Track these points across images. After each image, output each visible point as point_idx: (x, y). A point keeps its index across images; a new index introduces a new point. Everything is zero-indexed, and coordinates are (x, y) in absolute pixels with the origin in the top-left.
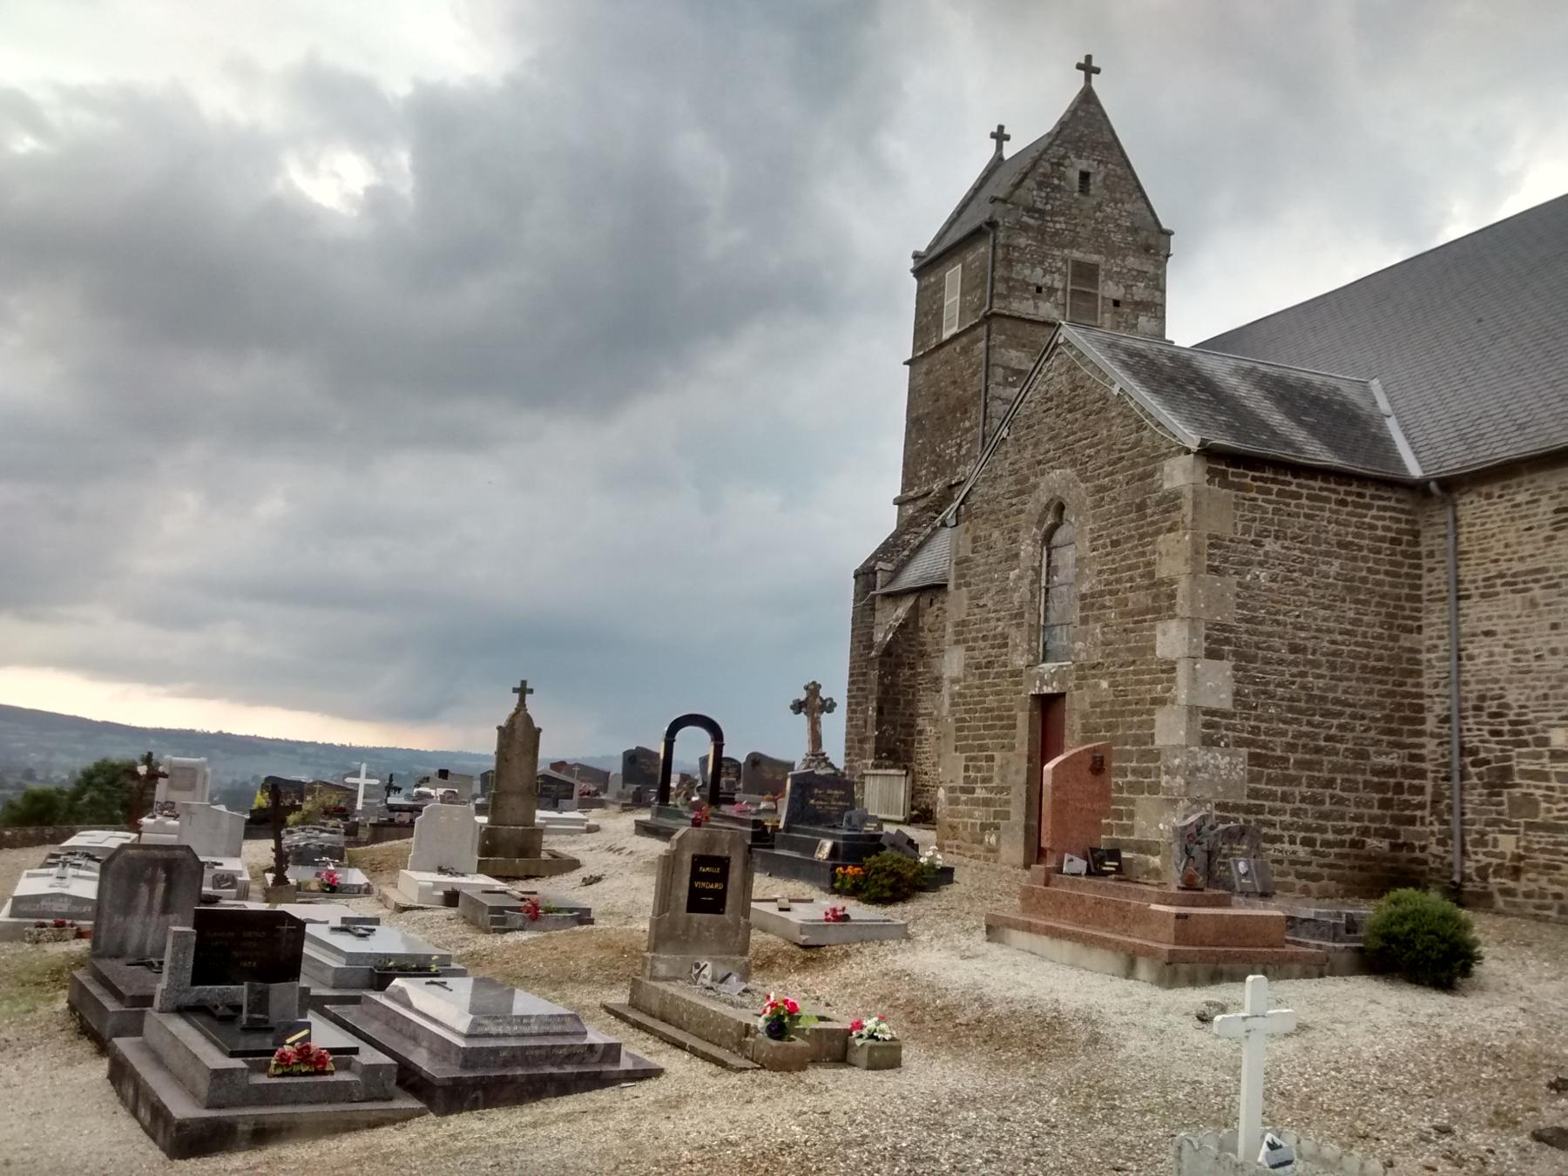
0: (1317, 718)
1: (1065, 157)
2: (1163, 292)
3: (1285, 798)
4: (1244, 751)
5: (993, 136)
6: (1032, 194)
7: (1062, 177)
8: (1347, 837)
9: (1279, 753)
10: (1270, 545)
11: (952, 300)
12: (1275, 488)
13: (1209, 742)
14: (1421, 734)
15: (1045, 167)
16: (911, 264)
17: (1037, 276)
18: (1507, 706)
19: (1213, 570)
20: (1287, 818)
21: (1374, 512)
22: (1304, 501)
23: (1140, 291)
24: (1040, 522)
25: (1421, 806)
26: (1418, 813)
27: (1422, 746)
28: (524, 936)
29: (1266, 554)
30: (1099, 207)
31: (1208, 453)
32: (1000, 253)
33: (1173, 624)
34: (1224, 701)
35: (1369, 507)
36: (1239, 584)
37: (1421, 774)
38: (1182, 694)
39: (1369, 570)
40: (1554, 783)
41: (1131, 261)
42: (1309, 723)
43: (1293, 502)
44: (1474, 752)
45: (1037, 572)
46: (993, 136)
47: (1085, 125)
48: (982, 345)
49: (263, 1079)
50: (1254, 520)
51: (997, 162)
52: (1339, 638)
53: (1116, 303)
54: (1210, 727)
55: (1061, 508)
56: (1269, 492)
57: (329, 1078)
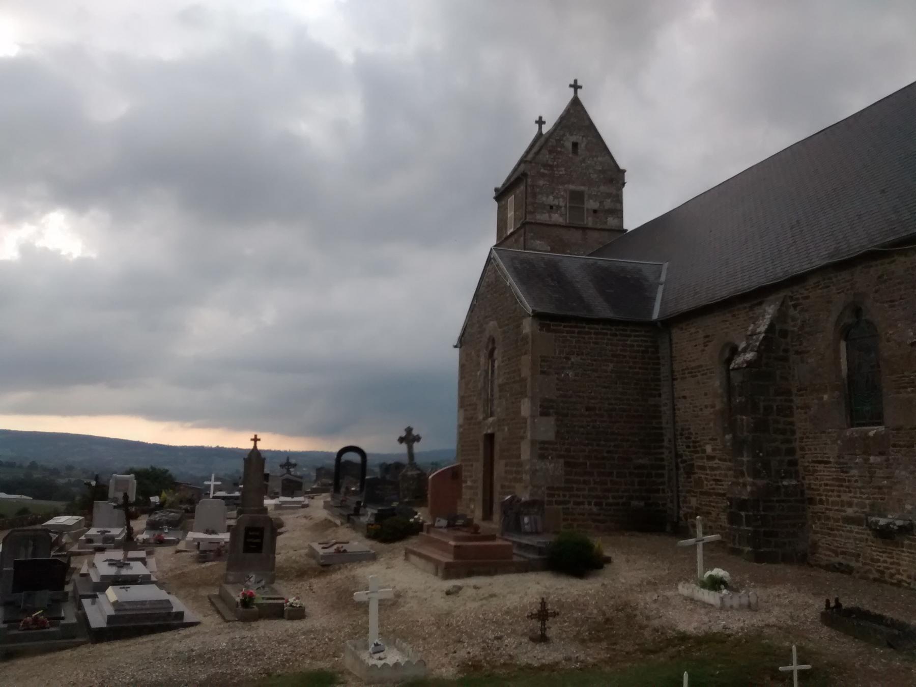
0: (602, 443)
1: (564, 135)
2: (621, 203)
3: (585, 482)
4: (562, 461)
5: (536, 122)
6: (546, 157)
7: (563, 146)
8: (621, 501)
9: (581, 460)
10: (573, 359)
11: (511, 214)
12: (576, 330)
13: (542, 457)
14: (661, 447)
15: (552, 142)
16: (494, 194)
17: (551, 200)
18: (691, 433)
19: (543, 372)
20: (586, 493)
21: (632, 338)
22: (593, 336)
23: (608, 204)
24: (487, 347)
25: (663, 483)
26: (661, 487)
27: (663, 453)
28: (214, 563)
29: (572, 363)
30: (583, 161)
31: (537, 316)
32: (529, 189)
33: (526, 400)
34: (550, 435)
35: (630, 336)
36: (558, 379)
37: (663, 467)
38: (529, 435)
39: (630, 367)
40: (708, 472)
41: (603, 188)
42: (598, 445)
43: (586, 337)
44: (681, 456)
45: (487, 372)
46: (536, 122)
47: (576, 118)
48: (522, 238)
49: (16, 632)
50: (565, 347)
51: (540, 134)
52: (613, 402)
53: (595, 211)
54: (543, 450)
55: (493, 341)
56: (574, 332)
57: (47, 630)
